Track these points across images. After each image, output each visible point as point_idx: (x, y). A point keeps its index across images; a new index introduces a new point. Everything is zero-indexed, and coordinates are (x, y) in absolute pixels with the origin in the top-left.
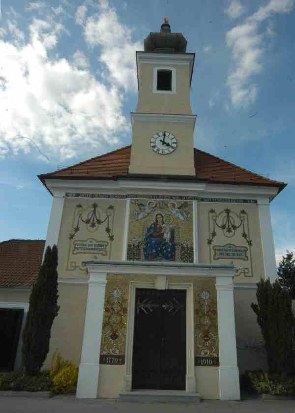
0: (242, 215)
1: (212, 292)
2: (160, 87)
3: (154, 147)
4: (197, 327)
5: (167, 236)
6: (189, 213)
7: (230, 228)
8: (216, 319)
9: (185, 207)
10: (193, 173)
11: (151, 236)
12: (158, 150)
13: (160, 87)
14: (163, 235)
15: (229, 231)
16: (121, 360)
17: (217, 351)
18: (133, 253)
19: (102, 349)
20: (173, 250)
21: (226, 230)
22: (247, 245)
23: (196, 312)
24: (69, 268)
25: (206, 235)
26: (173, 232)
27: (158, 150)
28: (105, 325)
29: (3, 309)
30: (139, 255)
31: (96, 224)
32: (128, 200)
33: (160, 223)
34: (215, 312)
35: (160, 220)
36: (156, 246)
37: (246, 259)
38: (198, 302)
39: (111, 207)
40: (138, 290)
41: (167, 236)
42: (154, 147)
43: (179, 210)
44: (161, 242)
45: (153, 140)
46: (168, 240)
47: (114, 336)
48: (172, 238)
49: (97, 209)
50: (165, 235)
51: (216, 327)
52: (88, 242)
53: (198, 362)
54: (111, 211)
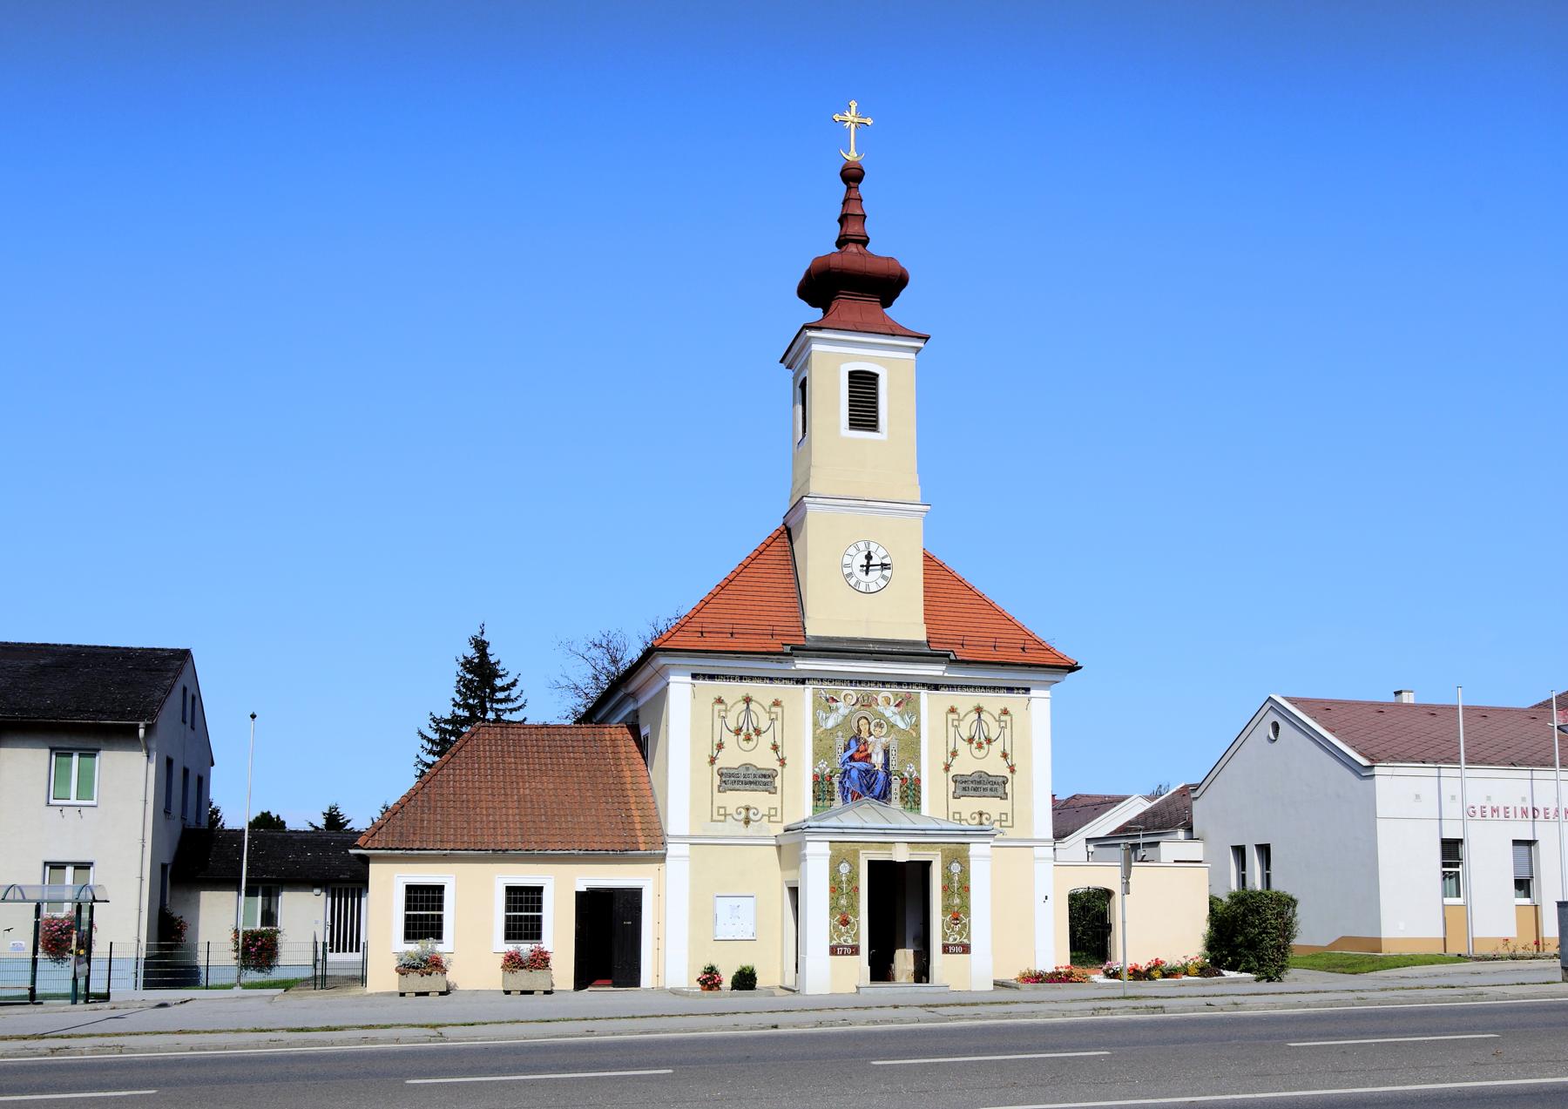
0: (1004, 718)
1: (964, 861)
2: (855, 423)
3: (847, 566)
4: (946, 909)
5: (878, 759)
6: (917, 712)
7: (980, 742)
8: (968, 897)
9: (907, 705)
10: (916, 631)
11: (852, 758)
12: (858, 582)
13: (855, 423)
14: (869, 756)
15: (980, 746)
16: (855, 950)
17: (968, 937)
18: (822, 789)
19: (832, 938)
20: (888, 784)
21: (975, 745)
22: (1007, 773)
23: (945, 889)
24: (716, 817)
25: (942, 758)
26: (886, 753)
27: (858, 582)
28: (833, 908)
29: (156, 924)
30: (831, 793)
31: (754, 737)
32: (809, 689)
33: (864, 735)
34: (967, 889)
35: (865, 727)
36: (863, 778)
37: (1004, 797)
38: (948, 877)
39: (776, 703)
40: (870, 862)
41: (878, 759)
42: (847, 566)
43: (896, 710)
44: (869, 773)
45: (847, 560)
46: (878, 767)
47: (845, 922)
48: (886, 763)
49: (753, 706)
50: (874, 757)
51: (968, 908)
52: (742, 771)
53: (946, 949)
54: (778, 710)
